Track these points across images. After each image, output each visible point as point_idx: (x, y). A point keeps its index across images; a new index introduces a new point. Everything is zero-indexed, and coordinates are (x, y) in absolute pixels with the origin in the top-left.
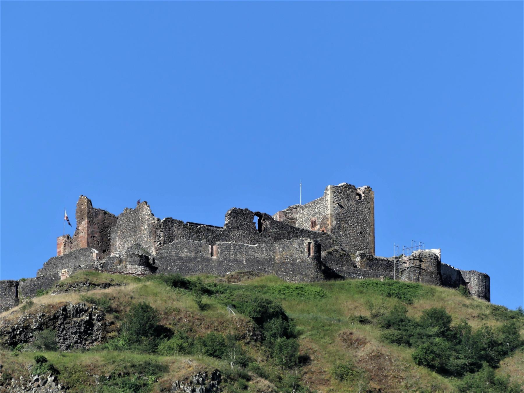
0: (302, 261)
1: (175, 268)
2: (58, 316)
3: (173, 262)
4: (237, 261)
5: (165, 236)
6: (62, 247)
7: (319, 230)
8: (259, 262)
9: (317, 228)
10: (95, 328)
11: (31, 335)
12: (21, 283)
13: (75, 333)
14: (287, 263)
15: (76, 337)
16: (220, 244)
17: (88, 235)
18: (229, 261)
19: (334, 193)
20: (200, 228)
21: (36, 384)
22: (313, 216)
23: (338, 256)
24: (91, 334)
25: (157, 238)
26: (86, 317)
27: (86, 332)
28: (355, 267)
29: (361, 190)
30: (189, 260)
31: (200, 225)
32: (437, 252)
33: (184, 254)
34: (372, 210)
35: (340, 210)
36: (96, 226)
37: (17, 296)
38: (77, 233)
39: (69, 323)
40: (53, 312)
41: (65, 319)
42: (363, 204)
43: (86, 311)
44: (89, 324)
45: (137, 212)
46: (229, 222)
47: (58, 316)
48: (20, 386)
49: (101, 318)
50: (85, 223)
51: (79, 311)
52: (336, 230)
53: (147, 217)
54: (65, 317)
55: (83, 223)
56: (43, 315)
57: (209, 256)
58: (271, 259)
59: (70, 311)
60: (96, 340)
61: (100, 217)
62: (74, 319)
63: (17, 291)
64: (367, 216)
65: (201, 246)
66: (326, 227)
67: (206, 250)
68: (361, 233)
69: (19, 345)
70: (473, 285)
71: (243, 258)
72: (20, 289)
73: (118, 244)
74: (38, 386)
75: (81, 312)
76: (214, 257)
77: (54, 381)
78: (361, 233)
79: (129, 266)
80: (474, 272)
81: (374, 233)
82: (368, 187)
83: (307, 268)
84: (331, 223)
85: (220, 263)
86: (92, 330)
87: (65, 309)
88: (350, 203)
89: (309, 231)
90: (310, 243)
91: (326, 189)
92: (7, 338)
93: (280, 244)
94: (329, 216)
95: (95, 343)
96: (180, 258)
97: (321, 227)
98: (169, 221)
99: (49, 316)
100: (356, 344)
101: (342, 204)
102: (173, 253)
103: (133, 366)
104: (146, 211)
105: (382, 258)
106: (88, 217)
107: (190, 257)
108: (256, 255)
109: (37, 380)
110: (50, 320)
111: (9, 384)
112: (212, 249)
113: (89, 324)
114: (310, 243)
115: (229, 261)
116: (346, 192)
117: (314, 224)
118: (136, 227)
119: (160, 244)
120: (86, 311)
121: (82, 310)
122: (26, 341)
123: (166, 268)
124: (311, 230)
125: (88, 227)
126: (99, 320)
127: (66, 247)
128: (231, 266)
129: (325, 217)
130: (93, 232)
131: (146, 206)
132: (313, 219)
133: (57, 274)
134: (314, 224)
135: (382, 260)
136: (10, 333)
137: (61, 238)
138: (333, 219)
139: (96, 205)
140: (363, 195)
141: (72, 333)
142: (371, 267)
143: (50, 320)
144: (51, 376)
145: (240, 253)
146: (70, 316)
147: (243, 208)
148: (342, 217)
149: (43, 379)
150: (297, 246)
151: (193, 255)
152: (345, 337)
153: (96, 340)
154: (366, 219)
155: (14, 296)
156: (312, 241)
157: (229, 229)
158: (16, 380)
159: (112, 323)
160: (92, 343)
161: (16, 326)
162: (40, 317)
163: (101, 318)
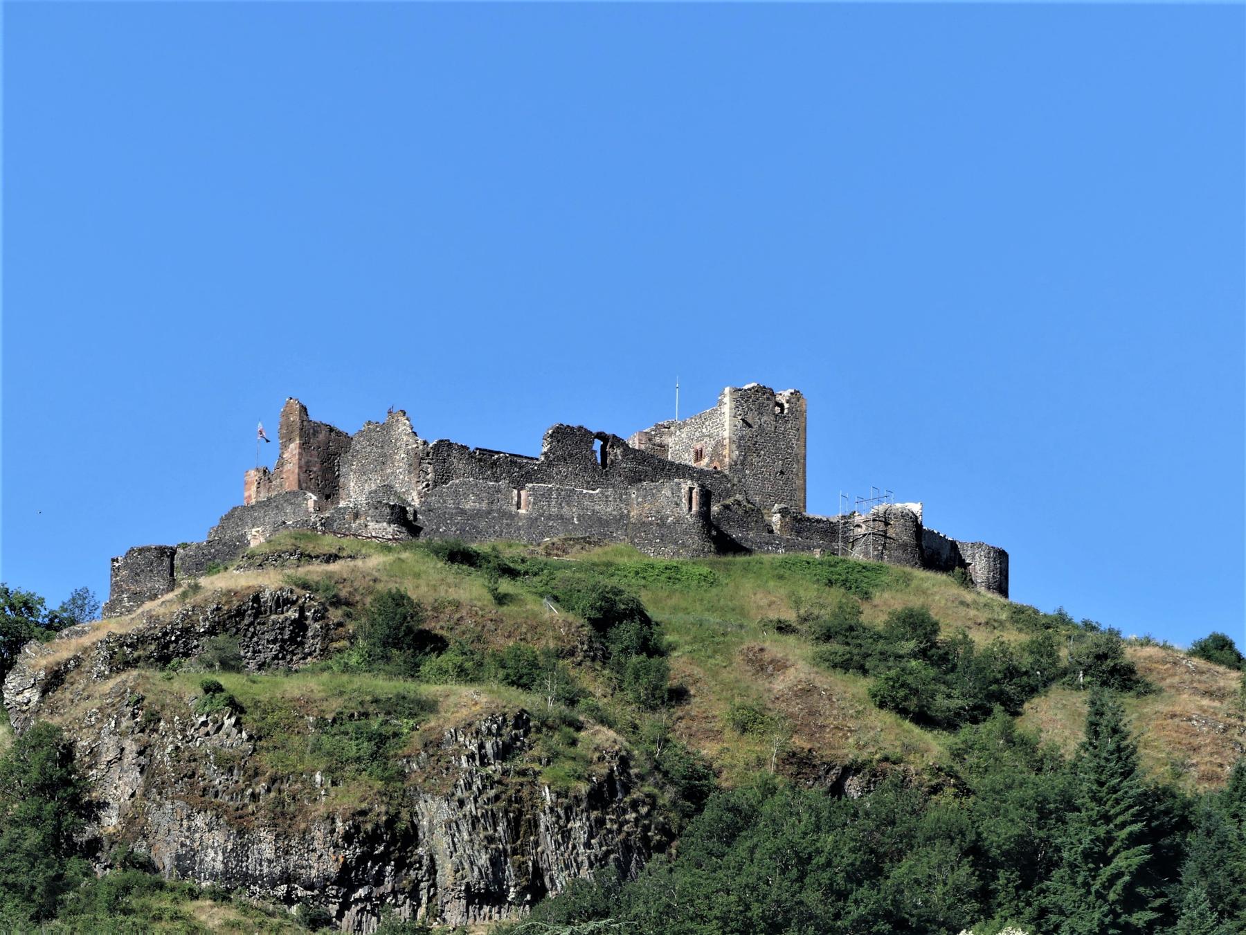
0: (678, 521)
1: (454, 529)
2: (245, 611)
3: (450, 519)
4: (562, 517)
5: (435, 471)
6: (254, 488)
7: (708, 465)
8: (601, 522)
9: (704, 463)
10: (310, 633)
11: (195, 643)
12: (180, 551)
13: (274, 641)
14: (651, 523)
15: (277, 647)
16: (533, 488)
17: (300, 467)
18: (549, 518)
19: (736, 400)
20: (498, 459)
21: (203, 730)
22: (698, 440)
23: (740, 512)
24: (302, 644)
25: (422, 475)
26: (293, 614)
27: (292, 640)
28: (771, 532)
29: (783, 396)
30: (478, 514)
31: (498, 453)
32: (915, 508)
33: (469, 505)
34: (802, 431)
35: (747, 431)
36: (315, 453)
37: (172, 575)
38: (281, 464)
39: (264, 624)
40: (235, 604)
41: (256, 617)
42: (786, 422)
43: (294, 603)
44: (300, 625)
45: (387, 428)
46: (550, 450)
47: (245, 611)
48: (174, 734)
49: (321, 616)
50: (294, 447)
51: (281, 603)
52: (739, 465)
53: (405, 438)
54: (258, 613)
55: (292, 446)
56: (218, 609)
57: (514, 509)
58: (622, 516)
59: (266, 602)
60: (310, 654)
61: (322, 436)
62: (273, 617)
63: (172, 565)
64: (794, 441)
65: (499, 491)
66: (721, 462)
67: (508, 499)
68: (782, 473)
69: (175, 661)
70: (978, 568)
71: (572, 512)
72: (177, 562)
73: (352, 484)
74: (207, 734)
75: (285, 604)
76: (522, 511)
77: (234, 726)
78: (782, 473)
79: (372, 525)
80: (981, 545)
81: (804, 472)
82: (796, 392)
83: (685, 532)
84: (729, 454)
85: (532, 521)
86: (304, 636)
87: (256, 599)
88: (765, 418)
89: (690, 468)
90: (691, 489)
91: (722, 394)
92: (153, 647)
93: (638, 490)
94: (726, 442)
95: (309, 659)
96: (463, 512)
97: (712, 461)
98: (444, 446)
99: (229, 611)
100: (770, 668)
101: (750, 421)
102: (450, 503)
103: (376, 701)
104: (403, 427)
105: (819, 517)
106: (301, 437)
107: (479, 510)
108: (597, 508)
109: (205, 724)
110: (230, 617)
111: (156, 731)
112: (519, 496)
113: (300, 625)
114: (691, 489)
115: (549, 518)
116: (756, 400)
117: (699, 455)
118: (385, 455)
119: (427, 485)
120: (294, 603)
121: (287, 602)
122: (186, 655)
123: (438, 529)
124: (695, 465)
125: (300, 454)
126: (316, 620)
127: (262, 489)
128: (552, 527)
129: (719, 444)
130: (308, 462)
131: (403, 419)
132: (698, 447)
133: (244, 536)
134: (699, 455)
135: (819, 521)
136: (158, 638)
137: (252, 473)
138: (734, 446)
139: (315, 416)
140: (786, 406)
141: (268, 642)
142: (798, 533)
143: (230, 617)
144: (229, 717)
145: (568, 504)
146: (265, 612)
147: (574, 424)
148: (748, 445)
149: (215, 722)
150: (669, 494)
151: (484, 506)
152: (751, 654)
153: (310, 654)
154: (792, 448)
155: (166, 575)
156: (696, 485)
157: (549, 464)
158: (167, 722)
159: (340, 625)
160: (304, 658)
161: (169, 627)
162: (212, 613)
163: (321, 616)
